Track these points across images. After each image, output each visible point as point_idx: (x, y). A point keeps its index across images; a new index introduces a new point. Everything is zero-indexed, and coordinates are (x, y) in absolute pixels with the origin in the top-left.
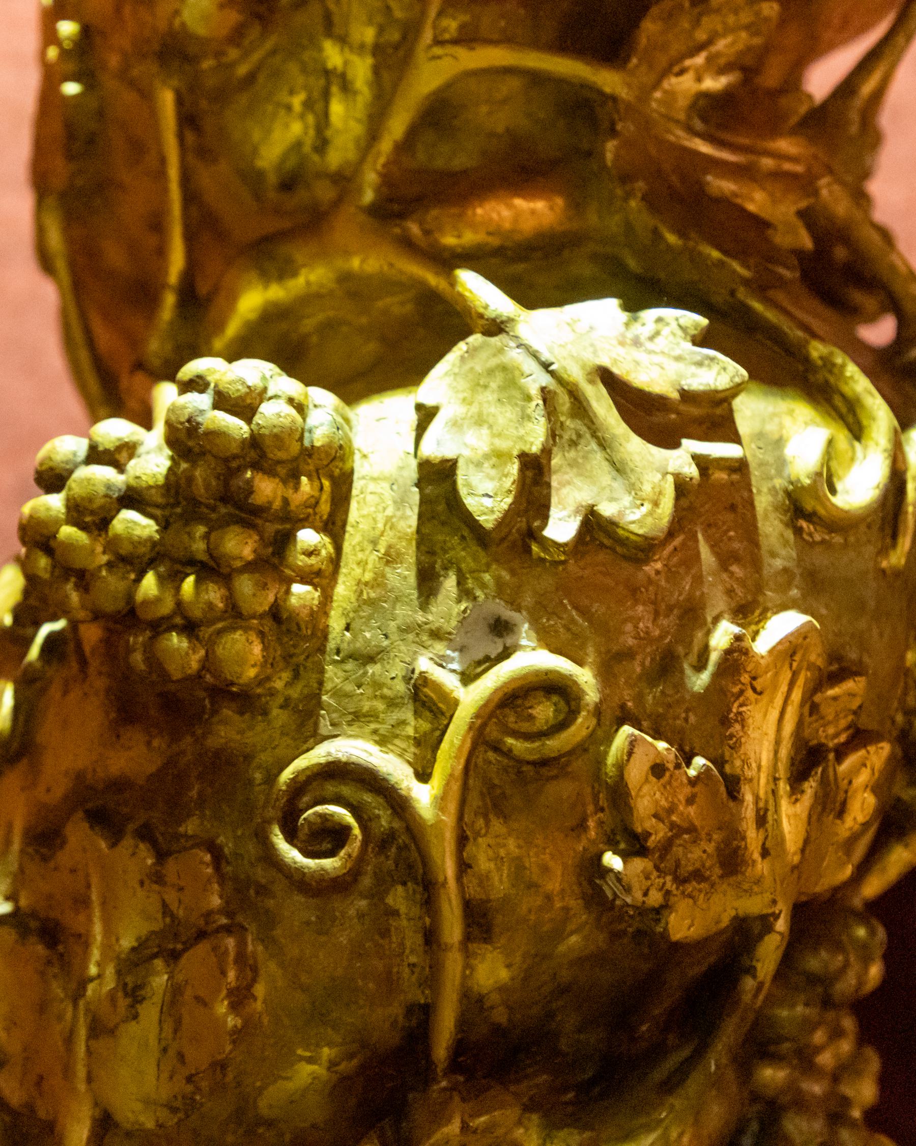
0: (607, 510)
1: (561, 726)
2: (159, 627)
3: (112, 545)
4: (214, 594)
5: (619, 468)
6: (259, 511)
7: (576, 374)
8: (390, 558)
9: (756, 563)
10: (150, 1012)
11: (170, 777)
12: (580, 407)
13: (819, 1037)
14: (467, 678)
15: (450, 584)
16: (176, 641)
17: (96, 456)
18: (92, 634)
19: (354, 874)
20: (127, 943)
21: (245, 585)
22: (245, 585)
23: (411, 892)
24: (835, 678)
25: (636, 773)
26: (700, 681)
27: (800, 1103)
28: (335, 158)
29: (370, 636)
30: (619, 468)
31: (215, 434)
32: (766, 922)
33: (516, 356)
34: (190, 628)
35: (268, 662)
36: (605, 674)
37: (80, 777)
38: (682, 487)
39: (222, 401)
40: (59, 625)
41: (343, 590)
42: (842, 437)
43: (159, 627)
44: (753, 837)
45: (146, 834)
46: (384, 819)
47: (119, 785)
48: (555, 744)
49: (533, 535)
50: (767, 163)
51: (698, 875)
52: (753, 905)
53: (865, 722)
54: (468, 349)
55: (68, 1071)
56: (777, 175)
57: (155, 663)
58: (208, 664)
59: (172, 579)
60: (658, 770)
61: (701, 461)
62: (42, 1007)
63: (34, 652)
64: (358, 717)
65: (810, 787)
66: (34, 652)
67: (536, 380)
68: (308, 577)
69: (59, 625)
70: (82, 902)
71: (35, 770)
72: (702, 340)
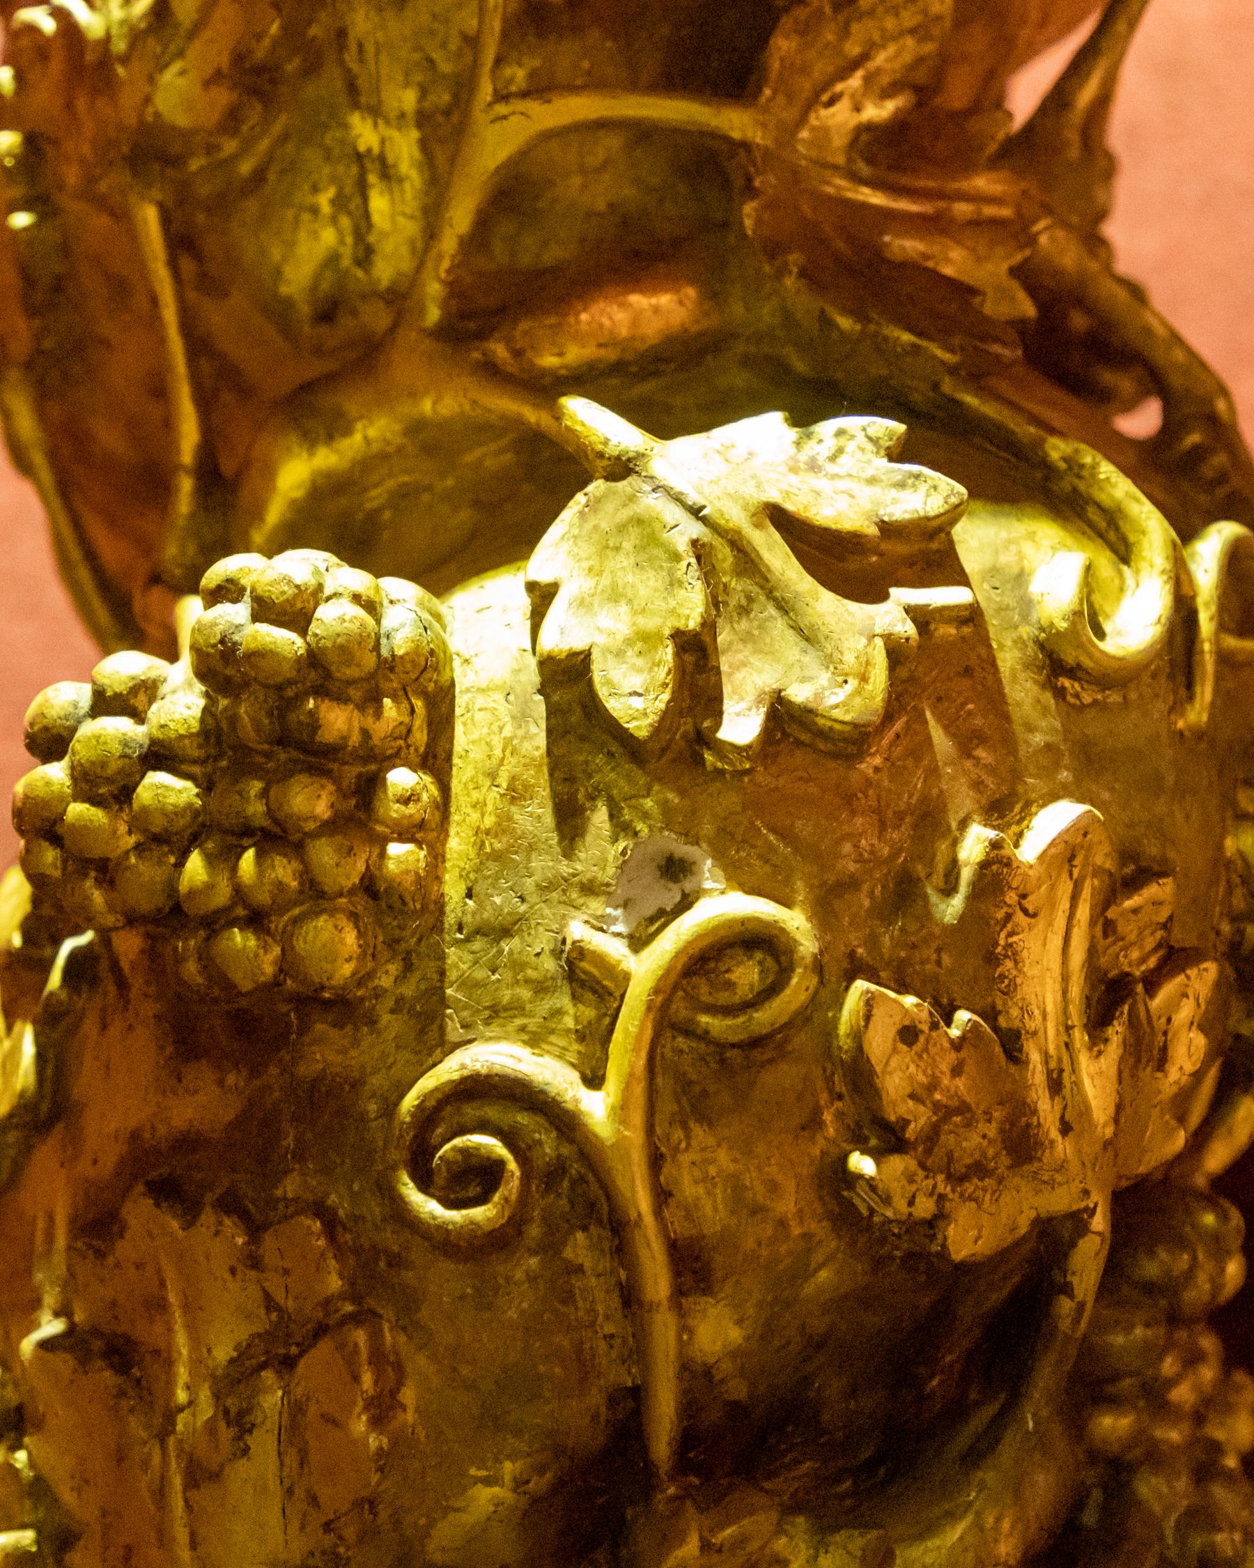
0: (799, 694)
1: (771, 990)
2: (214, 923)
3: (139, 822)
4: (284, 870)
5: (808, 636)
6: (333, 751)
7: (737, 517)
10: (264, 1443)
12: (748, 562)
14: (638, 942)
15: (600, 817)
16: (240, 939)
17: (104, 704)
19: (516, 1222)
20: (223, 1353)
21: (324, 853)
22: (324, 853)
24: (1132, 884)
25: (879, 1042)
26: (951, 909)
27: (1155, 1457)
28: (384, 272)
30: (808, 636)
31: (258, 655)
32: (1078, 1221)
33: (653, 504)
34: (256, 920)
35: (367, 952)
38: (896, 653)
39: (264, 610)
41: (457, 844)
42: (1105, 562)
43: (214, 923)
44: (1047, 1110)
45: (230, 1205)
46: (548, 1145)
47: (188, 1143)
48: (766, 1017)
49: (703, 740)
50: (963, 209)
51: (979, 1169)
52: (1059, 1201)
53: (1180, 937)
58: (287, 965)
59: (225, 858)
60: (908, 1034)
64: (496, 1013)
65: (1116, 1032)
66: (55, 979)
70: (158, 1306)
71: (75, 1140)
72: (901, 453)
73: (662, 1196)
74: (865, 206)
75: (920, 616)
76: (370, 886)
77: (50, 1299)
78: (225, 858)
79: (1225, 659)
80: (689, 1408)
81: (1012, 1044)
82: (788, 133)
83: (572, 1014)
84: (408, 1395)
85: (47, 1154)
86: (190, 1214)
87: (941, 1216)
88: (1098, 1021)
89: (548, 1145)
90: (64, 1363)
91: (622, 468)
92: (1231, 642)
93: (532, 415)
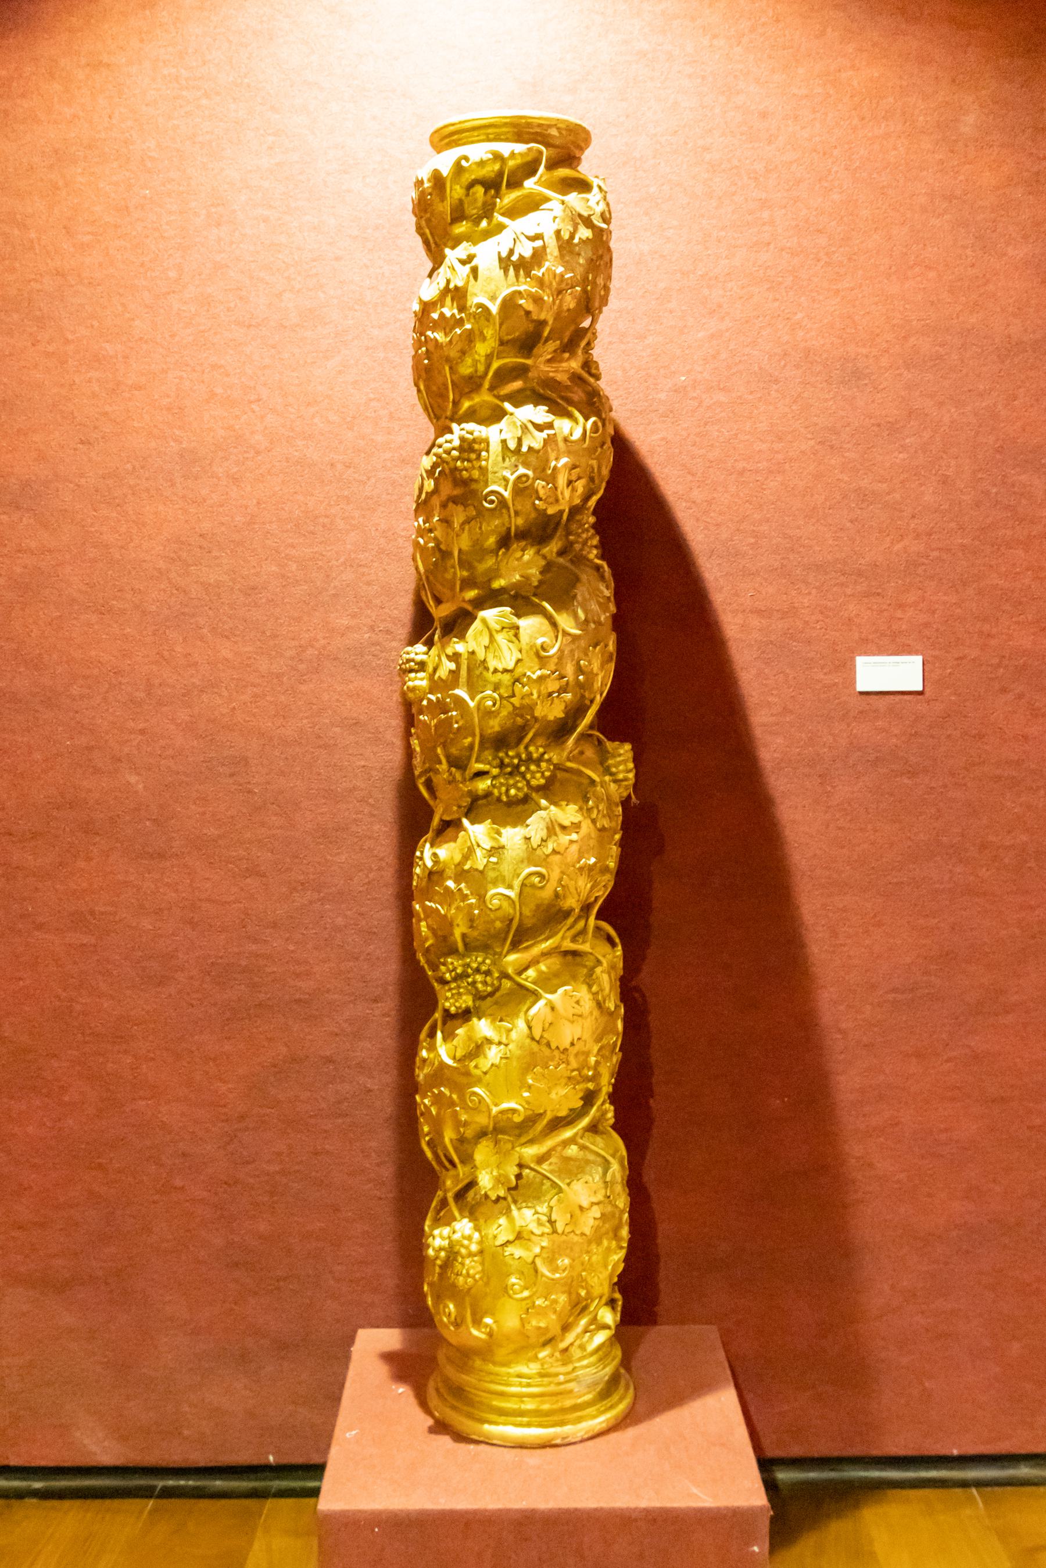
0: (532, 445)
1: (526, 482)
2: (462, 470)
3: (452, 457)
4: (470, 465)
5: (533, 437)
6: (476, 450)
7: (525, 422)
8: (497, 456)
9: (558, 450)
10: (466, 531)
11: (307, 541)
12: (526, 427)
13: (455, 453)
14: (512, 474)
15: (507, 459)
16: (464, 472)
17: (446, 442)
18: (447, 471)
19: (497, 507)
20: (461, 521)
21: (475, 462)
22: (475, 462)
23: (603, 1230)
24: (573, 469)
25: (540, 488)
26: (549, 472)
27: (577, 542)
28: (479, 374)
29: (495, 469)
30: (533, 437)
31: (467, 439)
32: (564, 510)
33: (515, 419)
34: (466, 470)
35: (480, 475)
36: (534, 472)
37: (449, 495)
38: (544, 440)
39: (468, 433)
40: (440, 469)
41: (490, 462)
42: (575, 424)
43: (462, 470)
44: (560, 497)
45: (462, 504)
46: (500, 498)
47: (456, 496)
48: (526, 485)
49: (520, 450)
50: (561, 369)
51: (551, 503)
52: (561, 508)
53: (581, 475)
54: (487, 669)
55: (453, 543)
56: (562, 371)
57: (461, 476)
58: (470, 475)
59: (463, 462)
60: (543, 487)
61: (548, 435)
62: (447, 534)
63: (437, 474)
64: (495, 482)
65: (570, 487)
66: (437, 474)
67: (519, 424)
68: (485, 460)
69: (440, 469)
70: (452, 516)
71: (439, 495)
72: (548, 412)
73: (513, 505)
74: (432, 1201)
75: (548, 435)
76: (480, 467)
77: (436, 515)
78: (463, 462)
79: (591, 437)
80: (516, 530)
81: (556, 488)
82: (535, 363)
83: (504, 483)
84: (173, 727)
85: (435, 497)
86: (457, 505)
87: (546, 509)
88: (568, 486)
89: (500, 498)
90: (439, 523)
91: (512, 414)
92: (592, 435)
93: (499, 403)
